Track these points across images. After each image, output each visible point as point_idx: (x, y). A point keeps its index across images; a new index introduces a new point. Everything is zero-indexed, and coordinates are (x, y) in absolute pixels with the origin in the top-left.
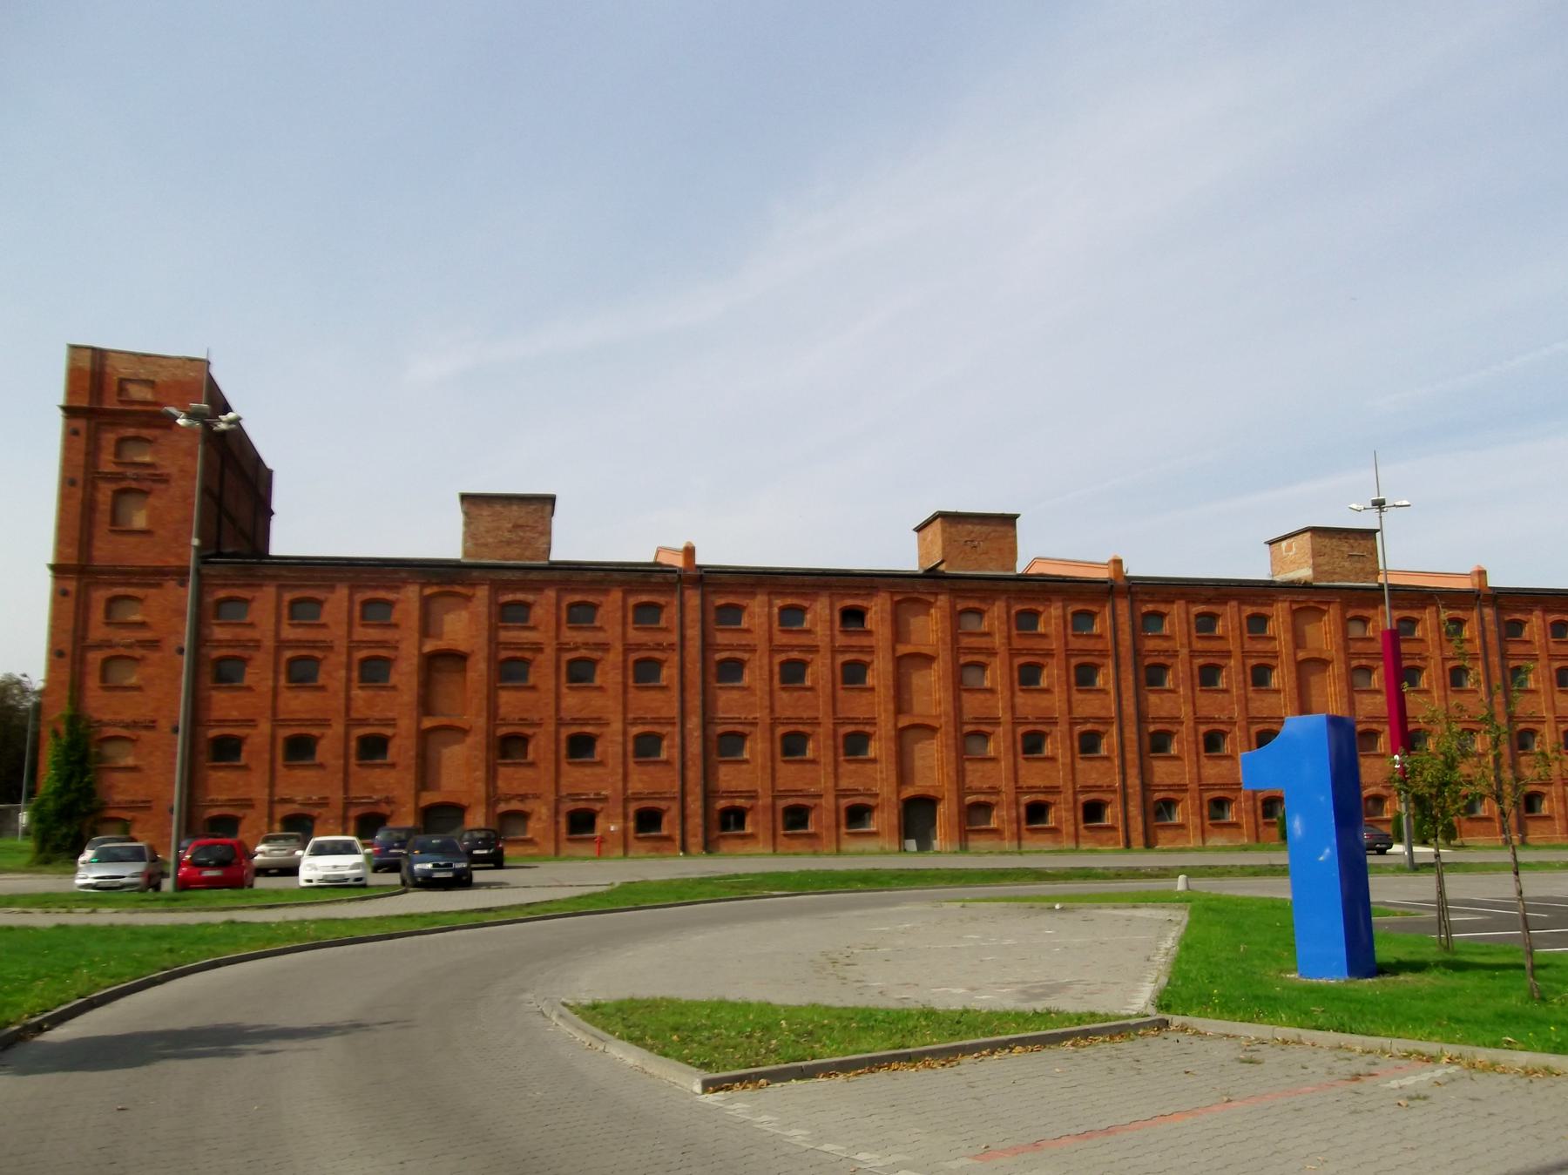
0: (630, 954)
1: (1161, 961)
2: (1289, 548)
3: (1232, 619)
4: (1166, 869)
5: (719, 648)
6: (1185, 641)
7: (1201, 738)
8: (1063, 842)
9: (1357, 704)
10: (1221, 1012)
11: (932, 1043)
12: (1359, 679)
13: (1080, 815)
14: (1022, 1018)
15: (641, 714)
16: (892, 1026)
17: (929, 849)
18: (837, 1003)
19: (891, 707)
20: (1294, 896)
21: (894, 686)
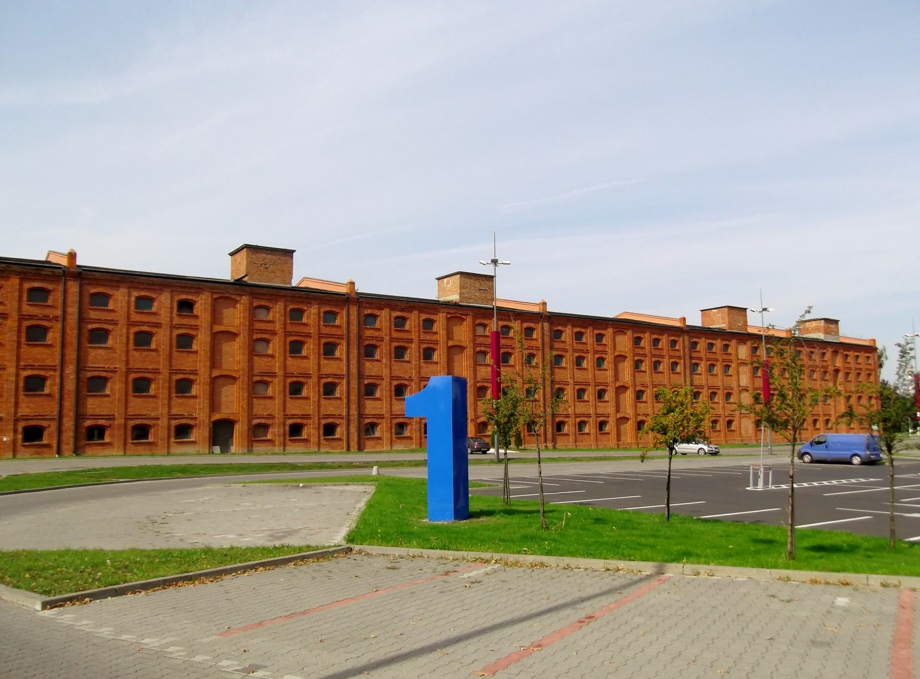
0: (6, 522)
1: (355, 514)
2: (448, 283)
3: (415, 321)
4: (368, 463)
5: (91, 321)
6: (388, 332)
7: (393, 388)
8: (310, 447)
9: (478, 372)
10: (382, 542)
11: (207, 568)
12: (480, 358)
13: (322, 432)
14: (265, 550)
15: (31, 362)
16: (182, 560)
17: (227, 452)
18: (148, 547)
19: (208, 364)
20: (429, 477)
21: (210, 350)
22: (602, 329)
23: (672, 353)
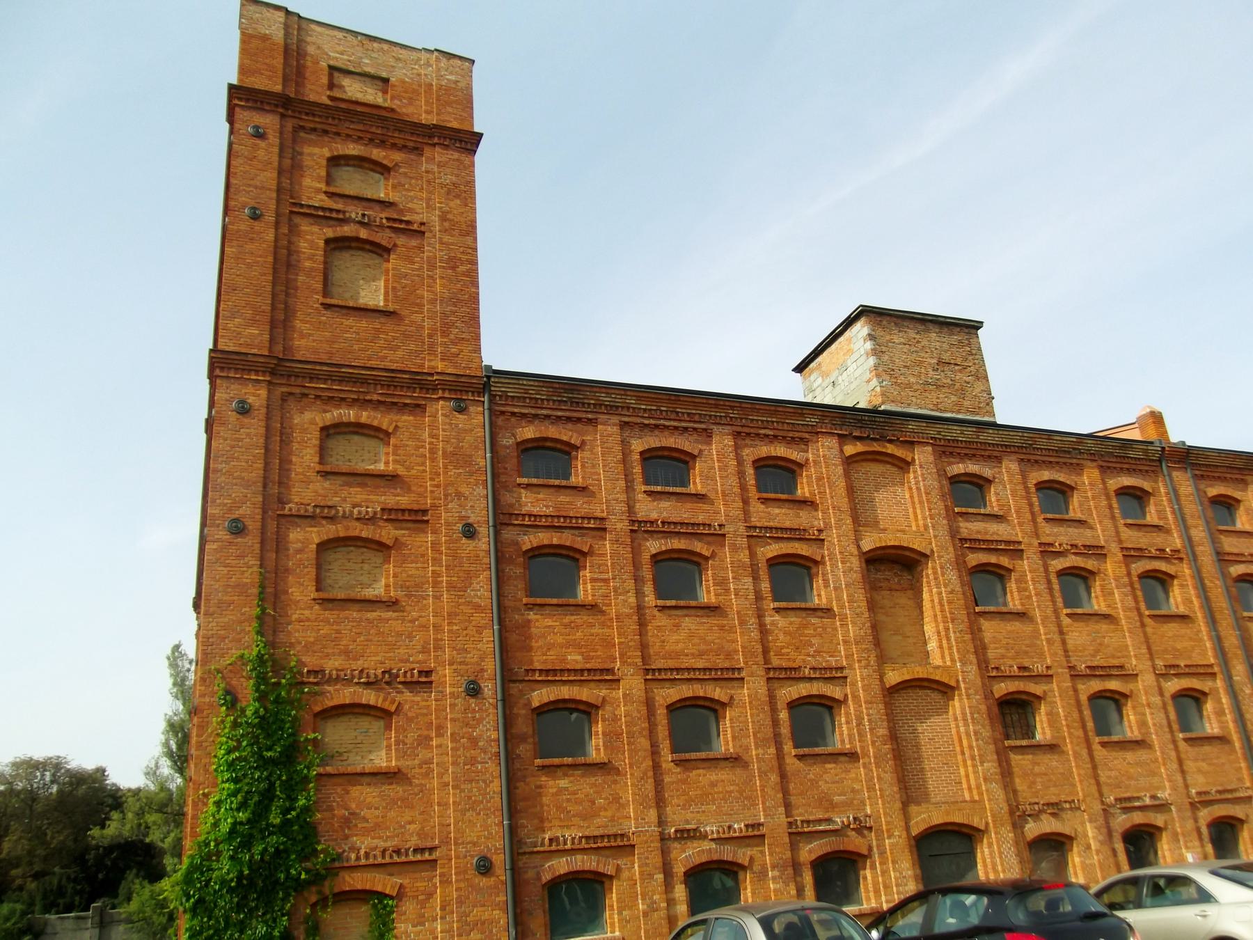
6: (736, 512)
22: (792, 441)
23: (1052, 534)
